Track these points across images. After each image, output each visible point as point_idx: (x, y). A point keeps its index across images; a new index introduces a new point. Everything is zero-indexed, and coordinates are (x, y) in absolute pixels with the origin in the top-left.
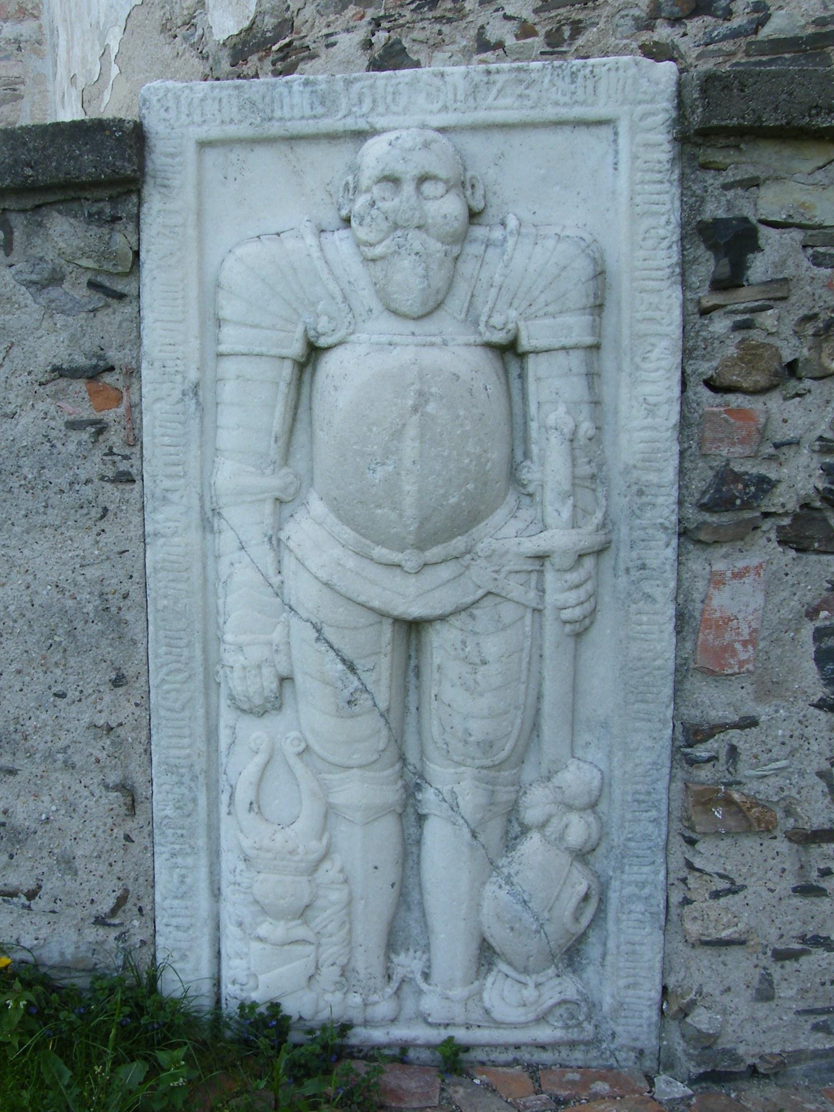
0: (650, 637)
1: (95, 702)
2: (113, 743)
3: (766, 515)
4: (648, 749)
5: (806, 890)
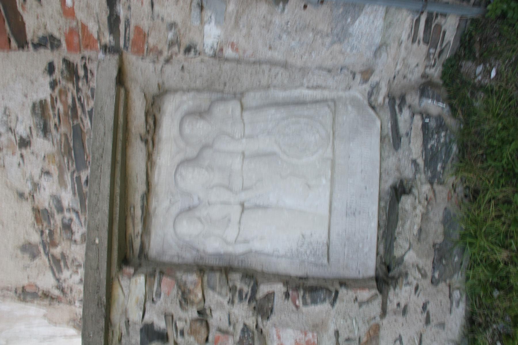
3: (257, 326)
5: (405, 312)
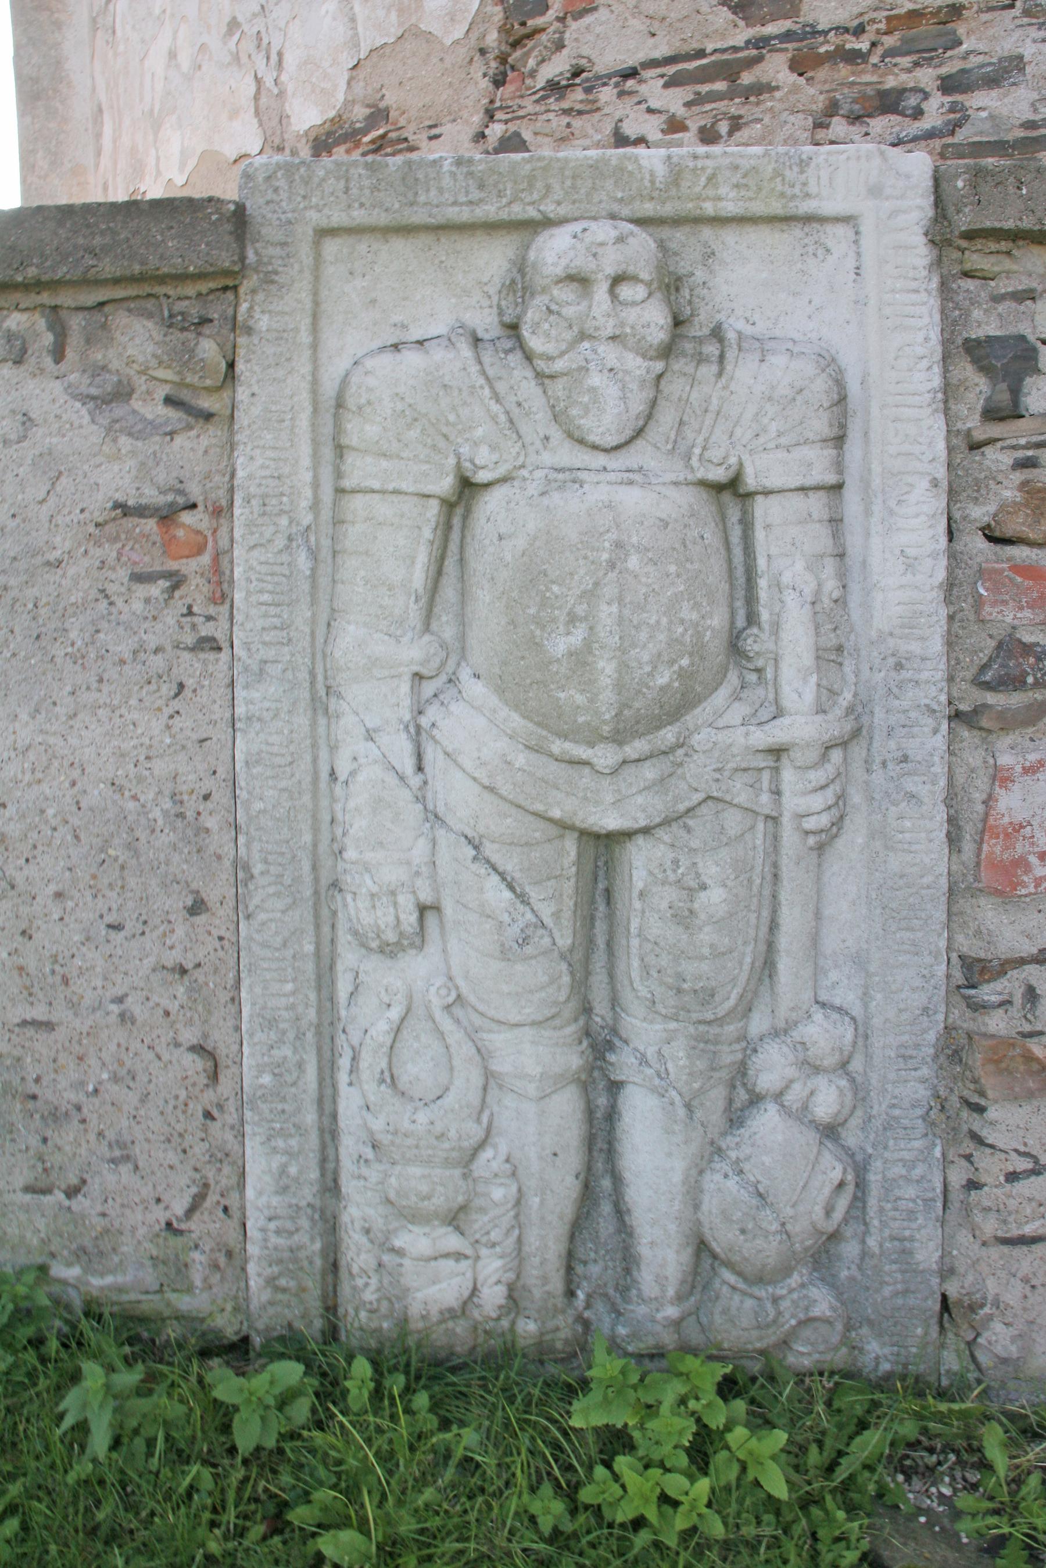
0: (914, 847)
1: (165, 935)
2: (190, 990)
4: (914, 990)
